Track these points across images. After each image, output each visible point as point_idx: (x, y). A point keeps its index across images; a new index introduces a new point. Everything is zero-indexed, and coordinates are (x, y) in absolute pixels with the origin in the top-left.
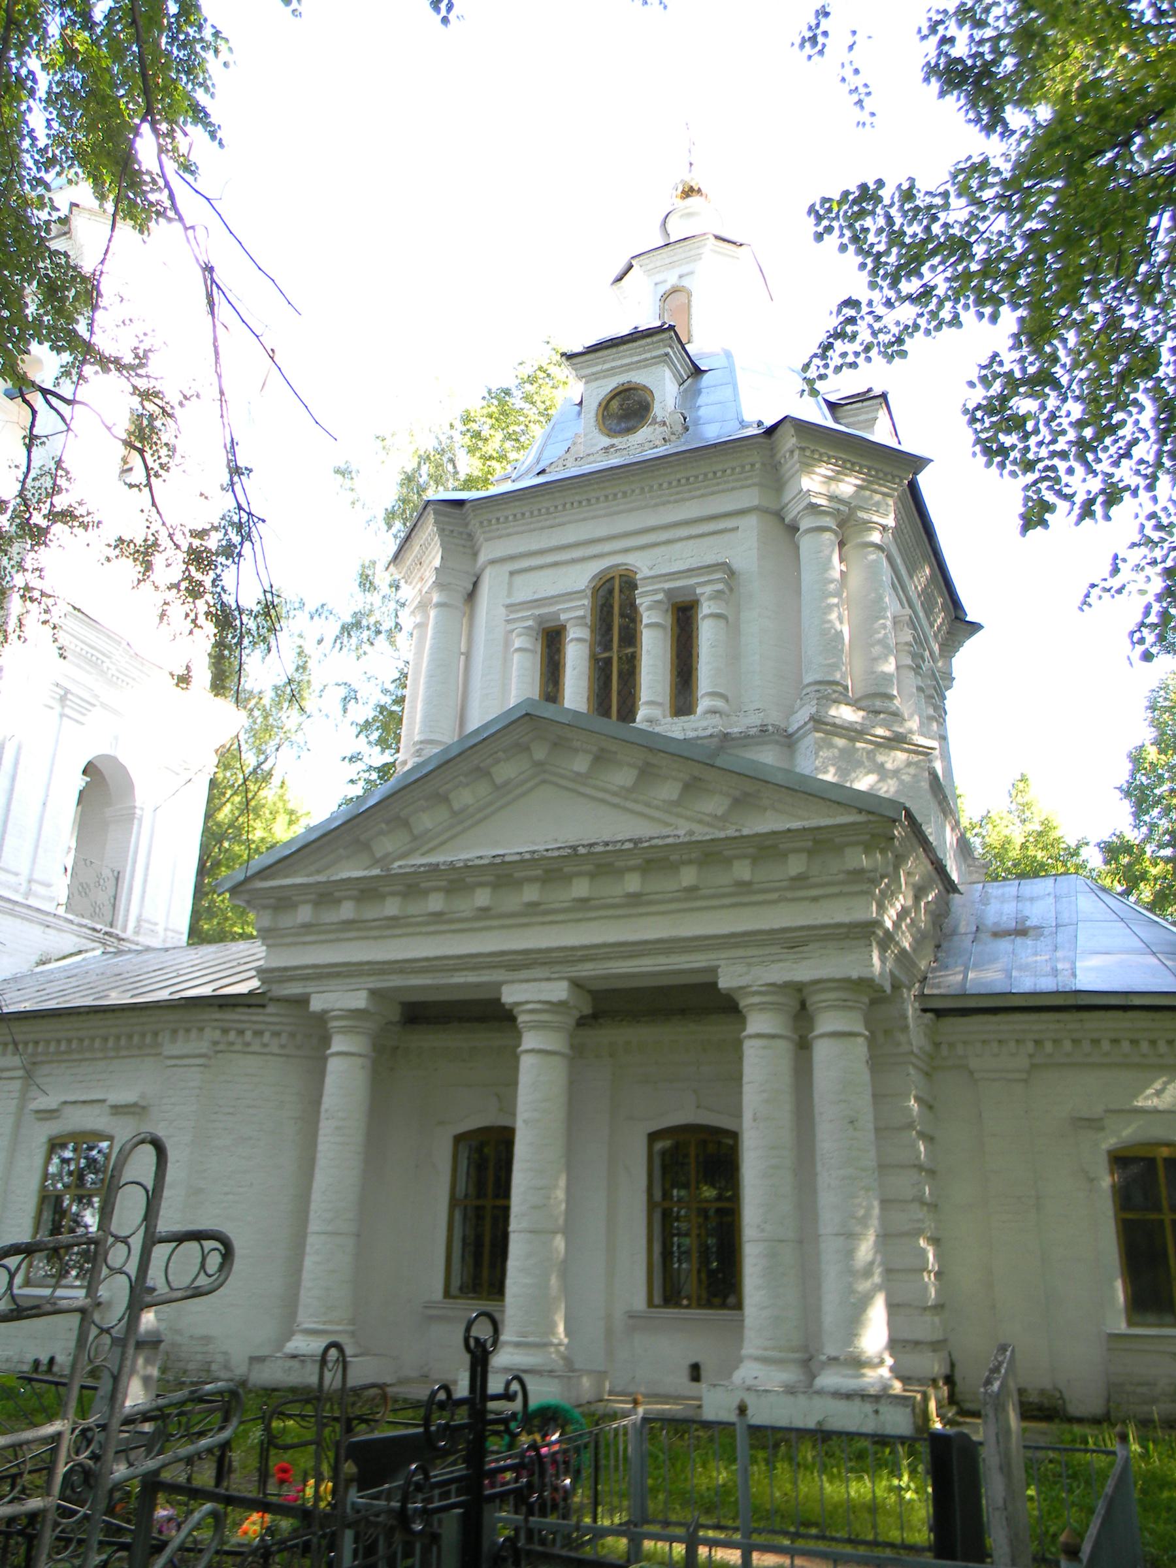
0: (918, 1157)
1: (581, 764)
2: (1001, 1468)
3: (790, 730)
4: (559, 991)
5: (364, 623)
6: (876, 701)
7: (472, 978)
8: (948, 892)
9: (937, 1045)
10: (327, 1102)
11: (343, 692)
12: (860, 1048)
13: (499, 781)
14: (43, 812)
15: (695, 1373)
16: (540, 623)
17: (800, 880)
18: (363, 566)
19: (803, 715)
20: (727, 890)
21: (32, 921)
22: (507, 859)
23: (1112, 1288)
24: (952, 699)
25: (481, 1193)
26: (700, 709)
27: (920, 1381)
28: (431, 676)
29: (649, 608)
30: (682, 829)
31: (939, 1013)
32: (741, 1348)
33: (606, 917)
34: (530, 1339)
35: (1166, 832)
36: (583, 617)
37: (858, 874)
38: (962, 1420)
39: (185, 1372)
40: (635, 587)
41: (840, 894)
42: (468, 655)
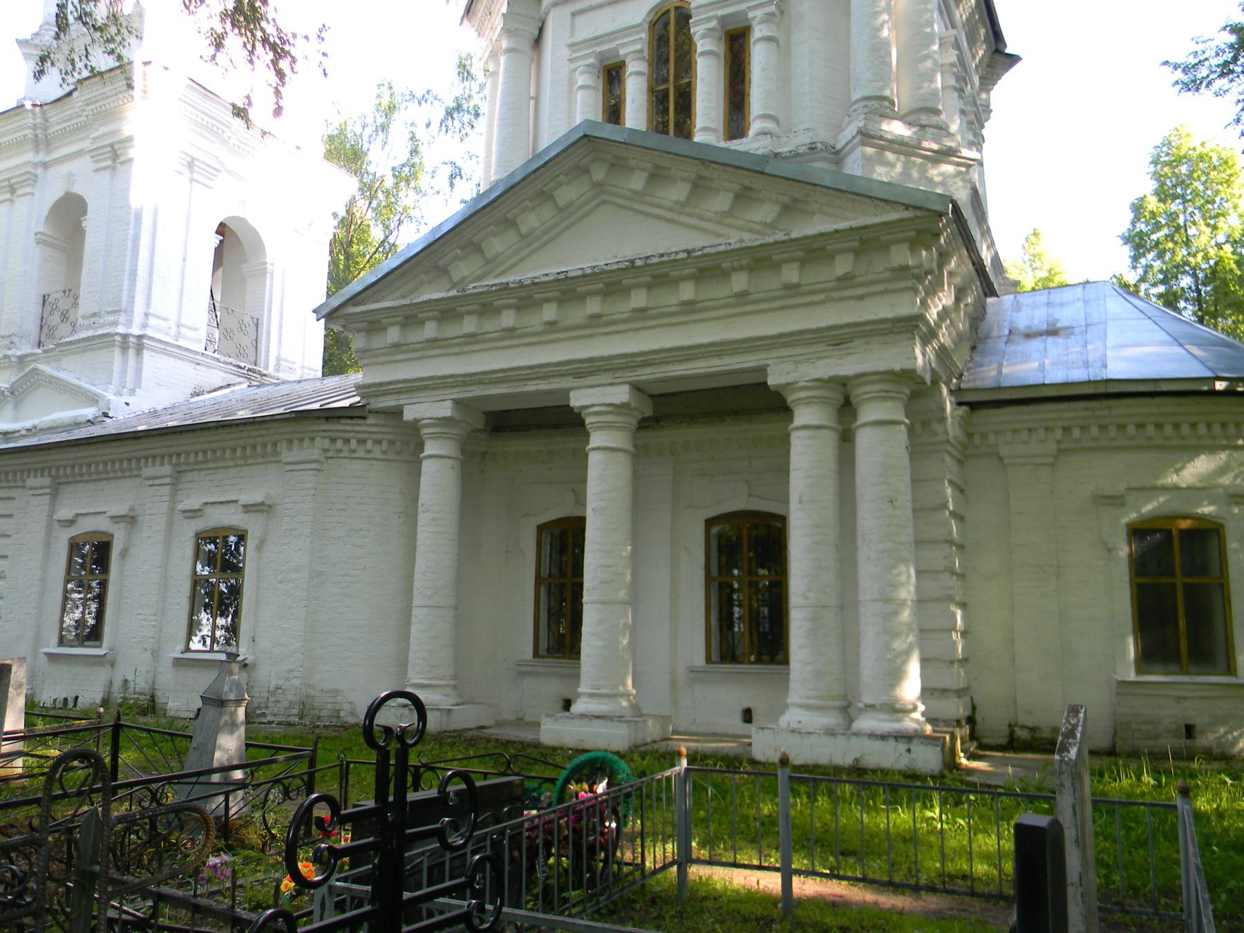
0: (950, 533)
1: (637, 182)
2: (1077, 841)
3: (838, 147)
4: (621, 394)
5: (465, 107)
6: (923, 114)
7: (543, 386)
8: (986, 295)
9: (970, 436)
10: (423, 498)
11: (448, 170)
12: (901, 433)
13: (561, 203)
14: (184, 265)
15: (748, 715)
16: (601, 61)
17: (846, 280)
18: (461, 58)
19: (850, 131)
20: (777, 293)
21: (183, 360)
22: (570, 275)
23: (1124, 643)
24: (989, 130)
25: (562, 574)
26: (752, 132)
27: (946, 722)
28: (502, 120)
29: (704, 37)
30: (734, 238)
31: (974, 406)
32: (787, 696)
33: (661, 325)
34: (603, 691)
35: (1161, 271)
36: (641, 51)
37: (902, 271)
38: (982, 753)
39: (319, 718)
40: (690, 17)
41: (886, 292)
42: (537, 99)
